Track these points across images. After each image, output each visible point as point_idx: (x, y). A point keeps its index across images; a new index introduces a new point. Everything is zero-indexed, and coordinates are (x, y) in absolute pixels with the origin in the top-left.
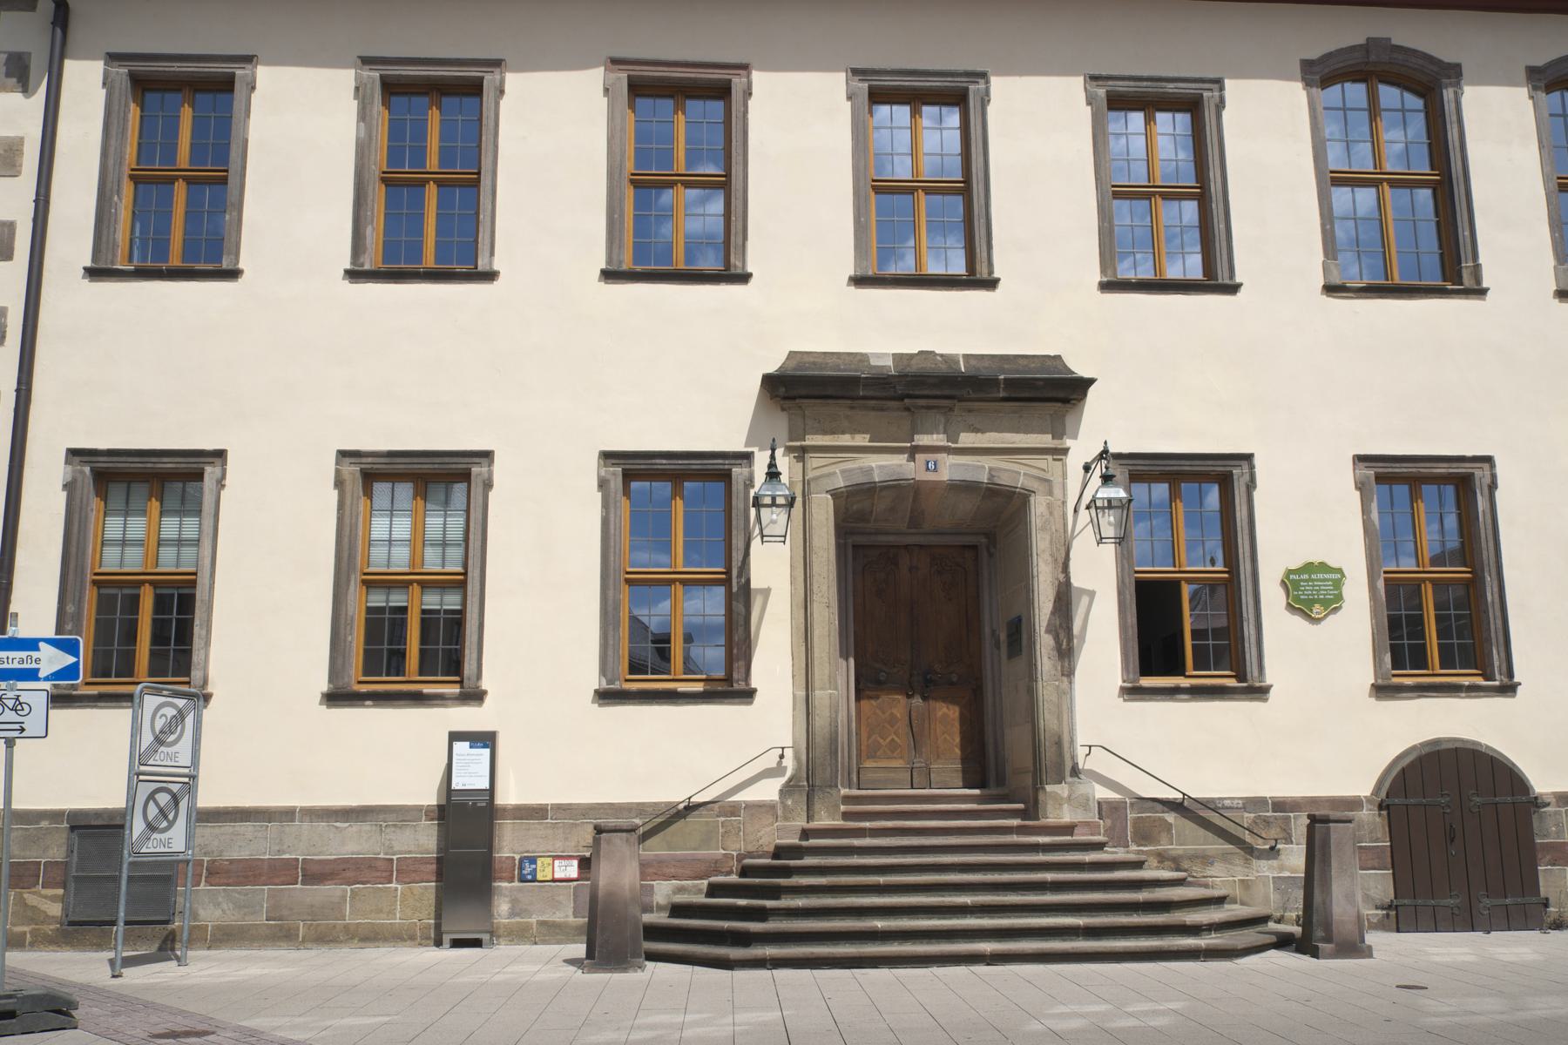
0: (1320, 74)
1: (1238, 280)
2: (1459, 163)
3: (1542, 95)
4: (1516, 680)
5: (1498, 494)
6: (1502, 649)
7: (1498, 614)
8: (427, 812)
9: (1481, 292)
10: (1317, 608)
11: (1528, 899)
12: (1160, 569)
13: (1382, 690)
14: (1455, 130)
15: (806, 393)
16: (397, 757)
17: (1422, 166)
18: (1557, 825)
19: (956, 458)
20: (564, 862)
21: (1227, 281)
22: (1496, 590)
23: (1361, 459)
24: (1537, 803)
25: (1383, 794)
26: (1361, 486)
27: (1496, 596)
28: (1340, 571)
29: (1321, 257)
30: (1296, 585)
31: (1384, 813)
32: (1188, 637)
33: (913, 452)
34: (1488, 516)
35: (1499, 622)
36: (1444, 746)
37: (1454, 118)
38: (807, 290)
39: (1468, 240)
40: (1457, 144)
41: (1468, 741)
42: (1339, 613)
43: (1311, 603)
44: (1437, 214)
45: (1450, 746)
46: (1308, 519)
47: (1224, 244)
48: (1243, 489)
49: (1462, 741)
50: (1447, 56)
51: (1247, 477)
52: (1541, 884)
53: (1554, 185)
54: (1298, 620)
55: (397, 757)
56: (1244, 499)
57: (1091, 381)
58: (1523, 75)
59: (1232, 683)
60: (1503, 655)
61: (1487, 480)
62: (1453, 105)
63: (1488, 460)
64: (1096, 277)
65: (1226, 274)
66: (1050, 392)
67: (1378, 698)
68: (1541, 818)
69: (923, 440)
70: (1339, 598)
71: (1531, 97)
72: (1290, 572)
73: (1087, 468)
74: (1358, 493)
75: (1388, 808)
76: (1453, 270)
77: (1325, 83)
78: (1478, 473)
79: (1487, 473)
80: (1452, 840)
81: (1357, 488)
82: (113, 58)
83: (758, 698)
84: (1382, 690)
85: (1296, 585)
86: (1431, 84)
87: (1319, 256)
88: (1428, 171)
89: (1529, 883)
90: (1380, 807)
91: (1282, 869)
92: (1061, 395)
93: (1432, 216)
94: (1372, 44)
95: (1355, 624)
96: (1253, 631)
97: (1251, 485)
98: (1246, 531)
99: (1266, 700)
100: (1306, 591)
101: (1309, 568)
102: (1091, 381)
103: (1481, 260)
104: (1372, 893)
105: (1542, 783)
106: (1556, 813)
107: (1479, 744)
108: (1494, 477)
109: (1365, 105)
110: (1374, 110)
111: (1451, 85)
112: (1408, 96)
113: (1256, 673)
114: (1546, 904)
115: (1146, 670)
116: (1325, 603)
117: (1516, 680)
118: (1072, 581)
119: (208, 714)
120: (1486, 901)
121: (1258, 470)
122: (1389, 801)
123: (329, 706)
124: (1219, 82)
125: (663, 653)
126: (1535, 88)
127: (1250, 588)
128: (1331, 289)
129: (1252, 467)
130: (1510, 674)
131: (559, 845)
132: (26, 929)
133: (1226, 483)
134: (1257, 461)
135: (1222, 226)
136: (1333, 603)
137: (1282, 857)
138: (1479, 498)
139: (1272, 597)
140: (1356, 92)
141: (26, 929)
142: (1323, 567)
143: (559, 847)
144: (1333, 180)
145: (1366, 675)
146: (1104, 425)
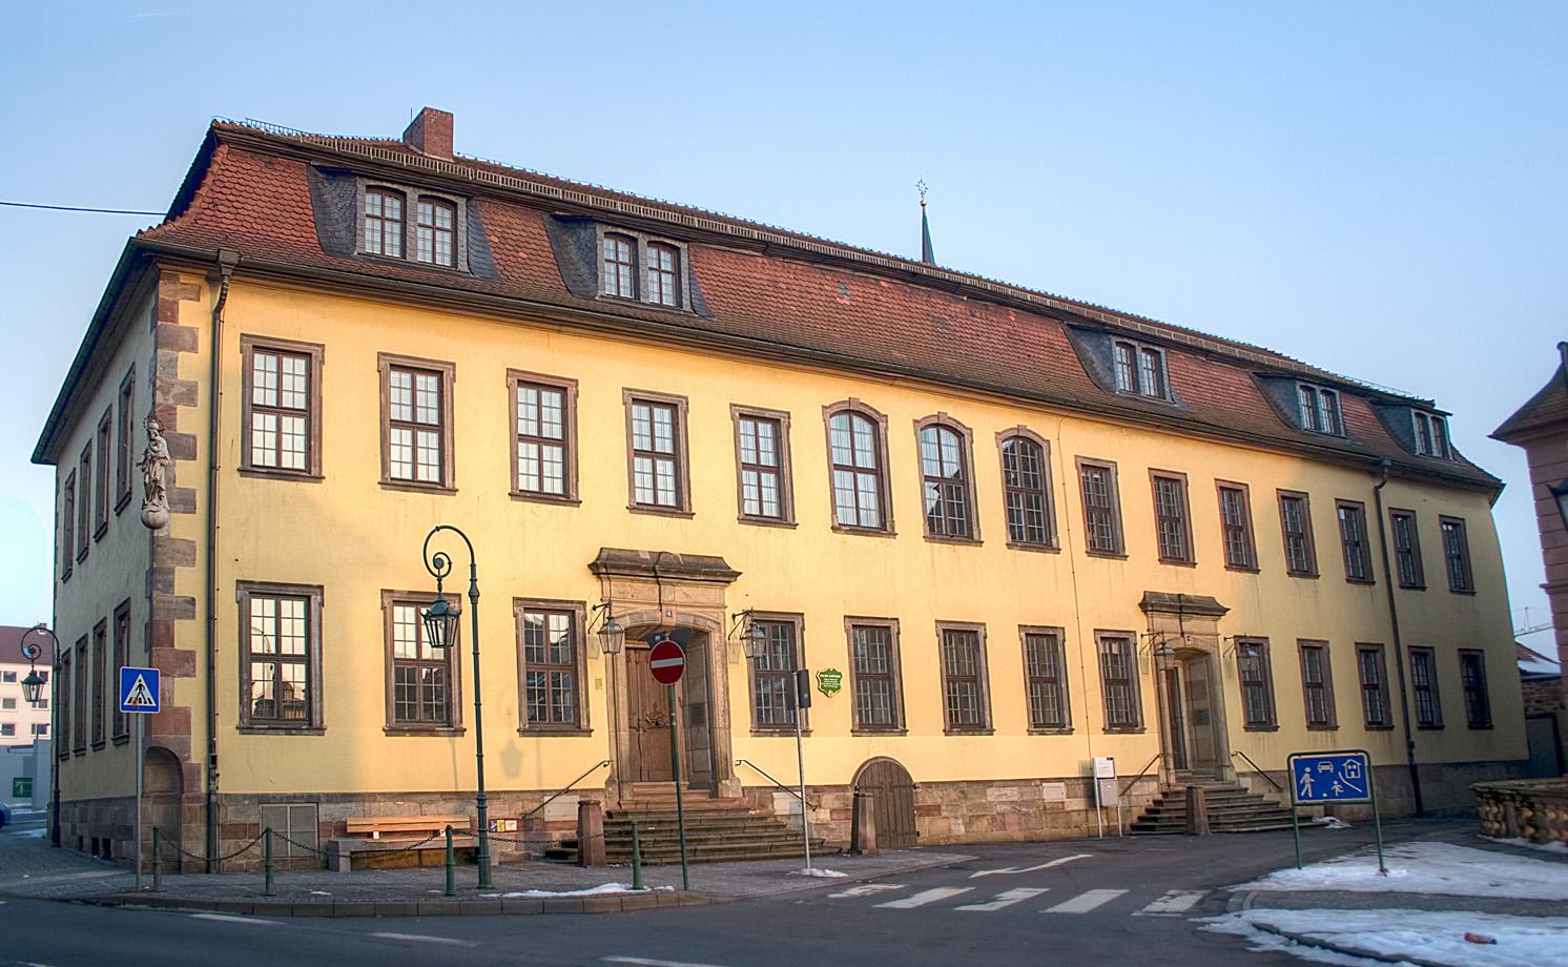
10: (830, 692)
15: (606, 566)
20: (510, 822)
32: (783, 703)
38: (609, 518)
43: (828, 689)
46: (826, 649)
51: (801, 625)
57: (1498, 435)
66: (717, 572)
70: (839, 687)
92: (727, 579)
95: (845, 698)
102: (1498, 435)
119: (851, 728)
125: (550, 704)
131: (507, 813)
132: (243, 862)
139: (846, 683)
141: (243, 862)
143: (507, 814)
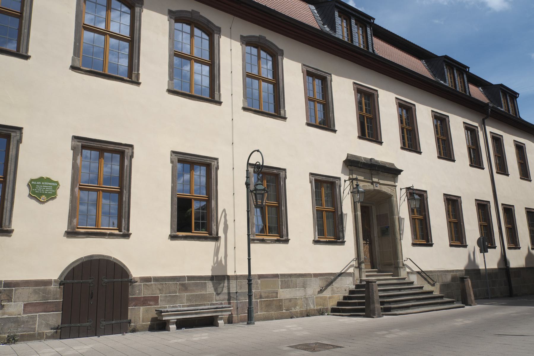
0: (247, 41)
1: (29, 54)
2: (138, 35)
3: (244, 46)
4: (130, 232)
5: (133, 160)
6: (126, 220)
7: (127, 206)
8: (55, 281)
9: (138, 84)
11: (122, 321)
12: (187, 195)
13: (173, 237)
14: (138, 23)
15: (352, 164)
16: (194, 258)
17: (270, 77)
18: (139, 290)
19: (383, 185)
21: (24, 54)
22: (127, 196)
23: (75, 138)
24: (132, 281)
25: (63, 279)
26: (74, 148)
27: (127, 199)
28: (57, 182)
29: (72, 55)
30: (34, 186)
31: (62, 287)
33: (372, 183)
34: (128, 168)
35: (127, 209)
36: (94, 258)
37: (138, 19)
39: (137, 64)
40: (138, 28)
41: (106, 256)
42: (55, 200)
43: (40, 195)
44: (274, 93)
45: (98, 258)
47: (26, 38)
48: (15, 142)
49: (103, 256)
50: (280, 47)
51: (18, 137)
52: (129, 314)
53: (172, 53)
54: (33, 202)
55: (194, 258)
56: (15, 146)
58: (167, 12)
59: (117, 232)
60: (127, 222)
61: (284, 176)
62: (138, 14)
63: (131, 146)
64: (70, 64)
65: (24, 51)
67: (68, 237)
68: (133, 287)
69: (375, 180)
70: (55, 194)
71: (169, 20)
72: (32, 180)
73: (345, 181)
74: (71, 152)
75: (63, 284)
76: (277, 111)
77: (177, 21)
78: (126, 151)
79: (130, 151)
80: (92, 298)
81: (72, 149)
82: (304, 65)
83: (131, 236)
84: (173, 237)
85: (34, 186)
86: (275, 55)
87: (71, 54)
88: (271, 78)
89: (124, 313)
90: (60, 285)
91: (4, 314)
93: (272, 92)
94: (260, 37)
96: (9, 205)
97: (20, 141)
98: (13, 160)
99: (10, 236)
100: (39, 189)
101: (41, 179)
102: (402, 171)
103: (140, 72)
104: (50, 323)
105: (136, 273)
106: (139, 285)
107: (111, 257)
108: (133, 153)
109: (256, 55)
110: (192, 35)
111: (139, 7)
112: (203, 34)
113: (7, 224)
114: (130, 322)
115: (179, 230)
116: (47, 195)
117: (130, 232)
118: (343, 211)
120: (104, 323)
121: (219, 164)
122: (65, 282)
123: (171, 240)
124: (330, 74)
126: (171, 18)
127: (11, 186)
128: (74, 68)
129: (286, 172)
130: (128, 230)
133: (122, 154)
134: (24, 131)
135: (26, 31)
136: (52, 196)
137: (5, 308)
138: (126, 160)
139: (21, 190)
140: (254, 51)
142: (49, 180)
144: (248, 75)
145: (167, 231)
146: (403, 182)
